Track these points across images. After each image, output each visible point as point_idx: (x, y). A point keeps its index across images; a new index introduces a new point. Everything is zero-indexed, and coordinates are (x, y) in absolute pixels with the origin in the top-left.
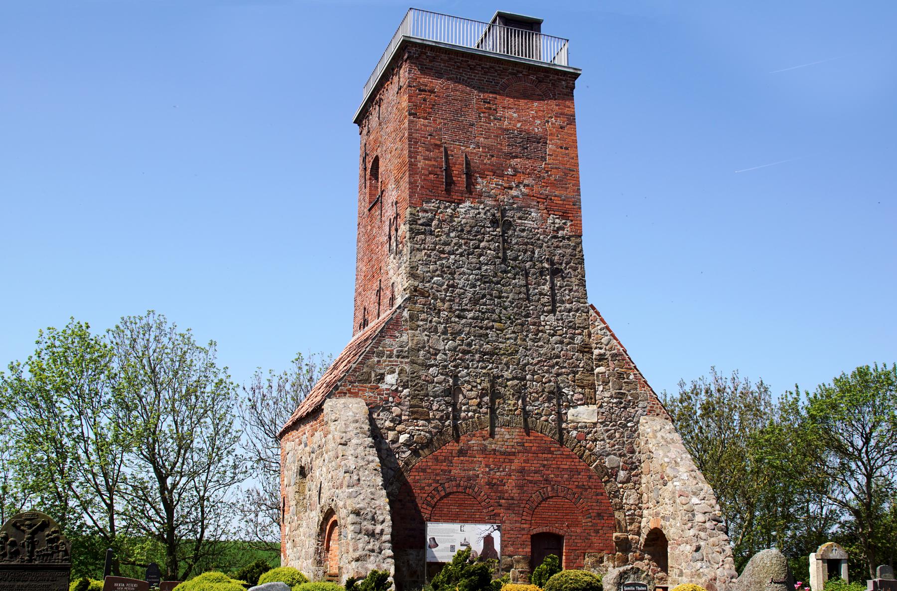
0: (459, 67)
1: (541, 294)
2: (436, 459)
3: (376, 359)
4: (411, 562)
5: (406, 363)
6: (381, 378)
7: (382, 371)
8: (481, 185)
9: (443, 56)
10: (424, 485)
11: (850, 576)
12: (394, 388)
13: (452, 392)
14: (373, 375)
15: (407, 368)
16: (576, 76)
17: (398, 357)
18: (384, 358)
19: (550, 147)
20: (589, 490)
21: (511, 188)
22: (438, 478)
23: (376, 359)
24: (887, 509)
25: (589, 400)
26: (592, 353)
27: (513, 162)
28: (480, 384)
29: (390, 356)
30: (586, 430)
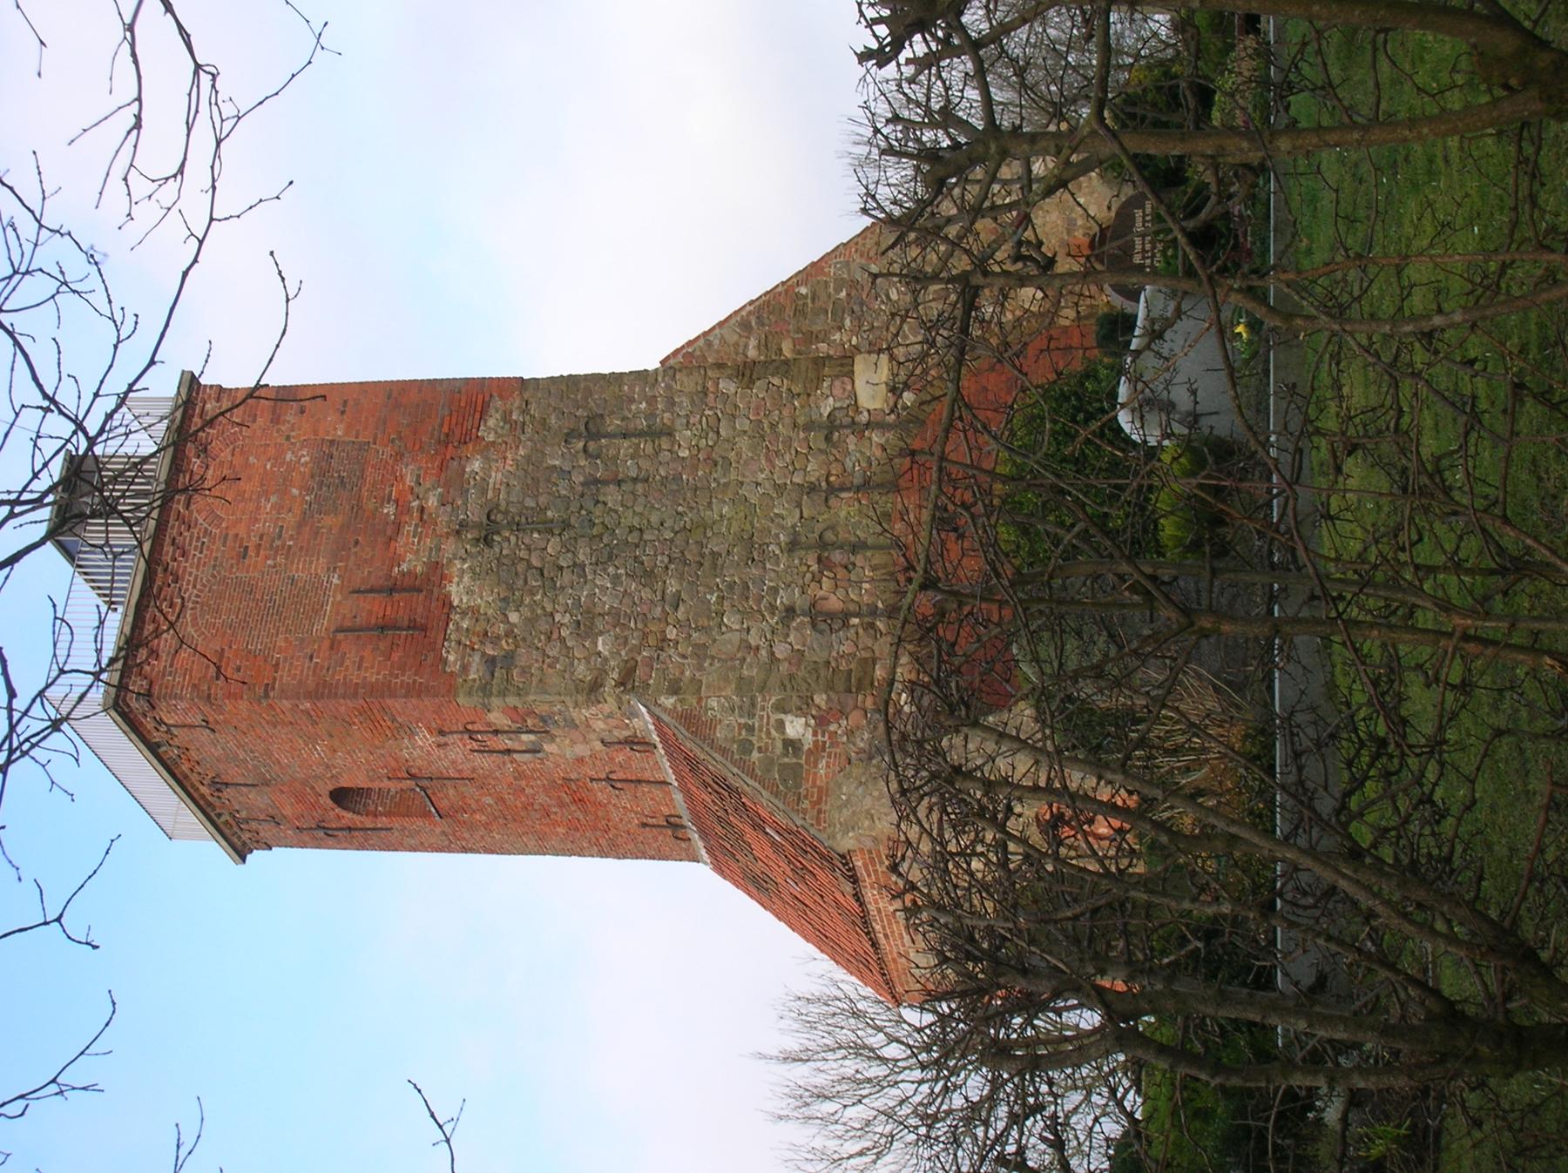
3: (755, 755)
6: (792, 745)
7: (779, 744)
17: (751, 715)
18: (754, 739)
25: (844, 365)
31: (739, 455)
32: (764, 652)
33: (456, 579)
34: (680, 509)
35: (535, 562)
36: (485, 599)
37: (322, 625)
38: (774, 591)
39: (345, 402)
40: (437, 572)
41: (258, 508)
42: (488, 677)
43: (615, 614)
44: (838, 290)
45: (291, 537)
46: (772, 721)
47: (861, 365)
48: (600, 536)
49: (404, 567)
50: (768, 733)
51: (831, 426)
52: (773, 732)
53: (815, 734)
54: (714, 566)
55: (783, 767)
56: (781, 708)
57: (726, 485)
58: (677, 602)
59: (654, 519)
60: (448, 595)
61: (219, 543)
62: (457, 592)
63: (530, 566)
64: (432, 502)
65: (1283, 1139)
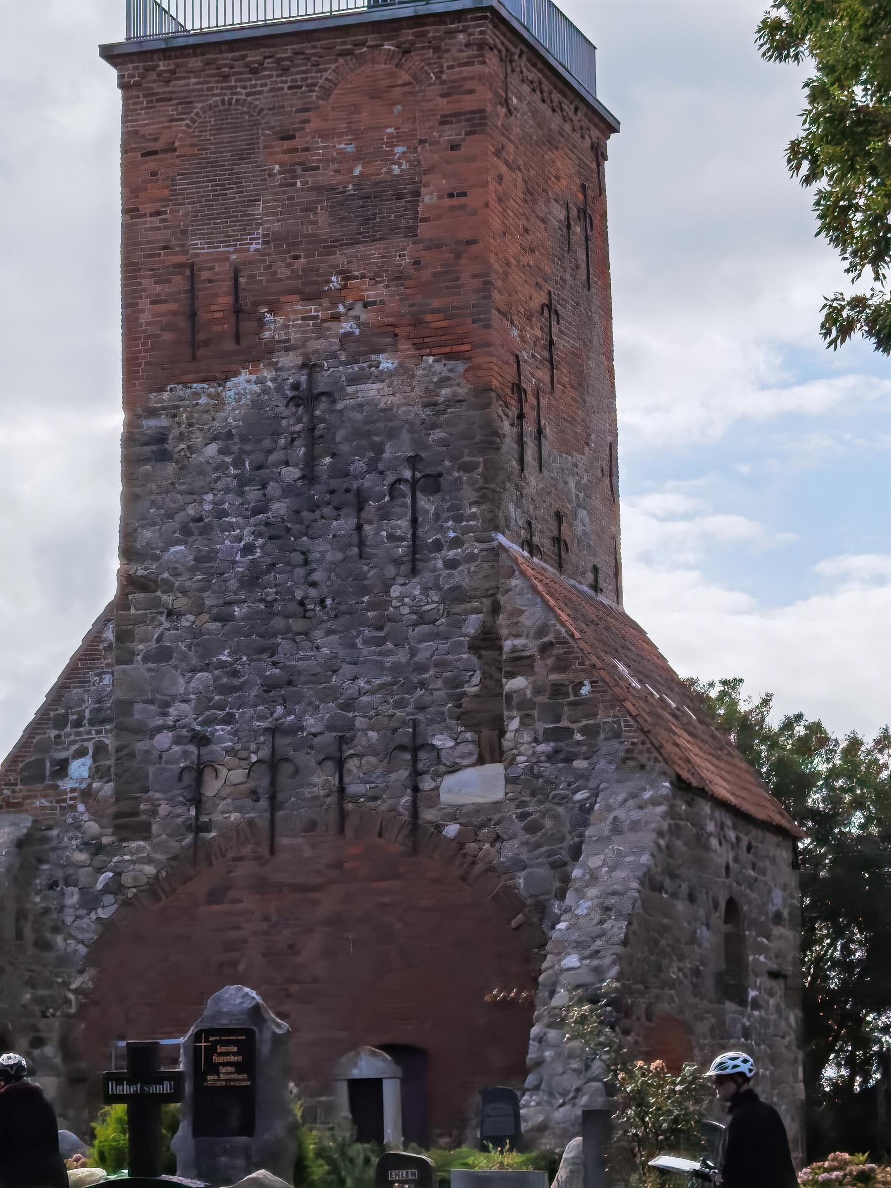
0: (226, 77)
1: (391, 537)
3: (53, 733)
5: (107, 731)
6: (62, 767)
7: (63, 755)
8: (274, 327)
9: (195, 63)
15: (109, 741)
16: (616, 131)
17: (92, 723)
18: (68, 729)
19: (428, 198)
21: (336, 318)
23: (53, 733)
25: (491, 752)
26: (500, 648)
27: (340, 258)
28: (255, 753)
29: (78, 724)
30: (478, 820)
31: (389, 653)
32: (159, 722)
33: (253, 378)
34: (329, 602)
35: (273, 458)
36: (232, 415)
37: (199, 248)
38: (229, 720)
39: (464, 194)
40: (263, 354)
41: (340, 135)
42: (144, 439)
43: (210, 556)
44: (584, 730)
45: (304, 183)
46: (85, 744)
47: (495, 770)
48: (300, 521)
49: (269, 317)
50: (73, 742)
51: (417, 746)
52: (75, 747)
53: (73, 790)
54: (262, 651)
55: (40, 763)
56: (100, 750)
57: (354, 646)
58: (224, 618)
59: (316, 576)
60: (237, 374)
61: (299, 104)
62: (244, 383)
63: (270, 452)
64: (346, 326)
65: (711, 1088)
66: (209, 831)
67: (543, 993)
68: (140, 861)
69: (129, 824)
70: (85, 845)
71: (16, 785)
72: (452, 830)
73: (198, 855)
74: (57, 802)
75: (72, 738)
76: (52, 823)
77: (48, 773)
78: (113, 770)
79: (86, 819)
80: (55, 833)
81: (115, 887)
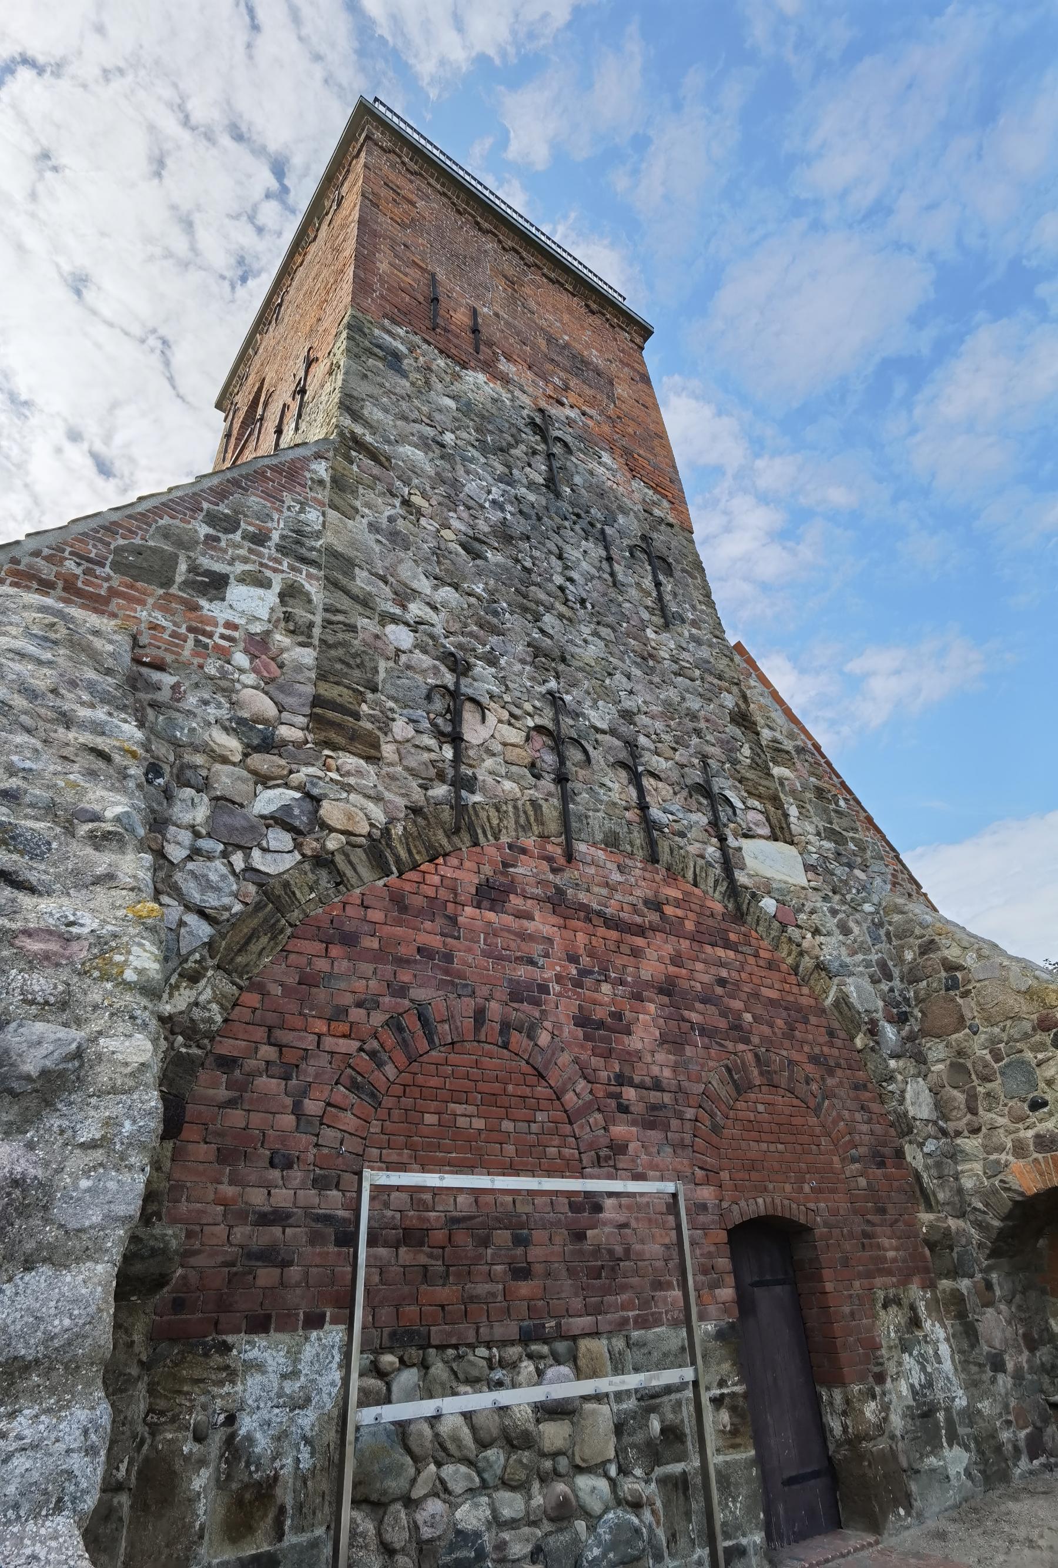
2: (398, 901)
4: (247, 1424)
10: (348, 999)
11: (679, 1461)
12: (257, 628)
13: (453, 706)
14: (183, 567)
20: (839, 1072)
22: (405, 976)
24: (886, 1242)
56: (290, 593)
66: (473, 792)
67: (246, 1337)
68: (360, 800)
69: (336, 723)
70: (240, 726)
71: (103, 566)
72: (769, 904)
73: (452, 819)
74: (190, 629)
75: (242, 552)
76: (169, 658)
77: (179, 579)
78: (317, 631)
79: (249, 682)
80: (167, 680)
81: (303, 823)
